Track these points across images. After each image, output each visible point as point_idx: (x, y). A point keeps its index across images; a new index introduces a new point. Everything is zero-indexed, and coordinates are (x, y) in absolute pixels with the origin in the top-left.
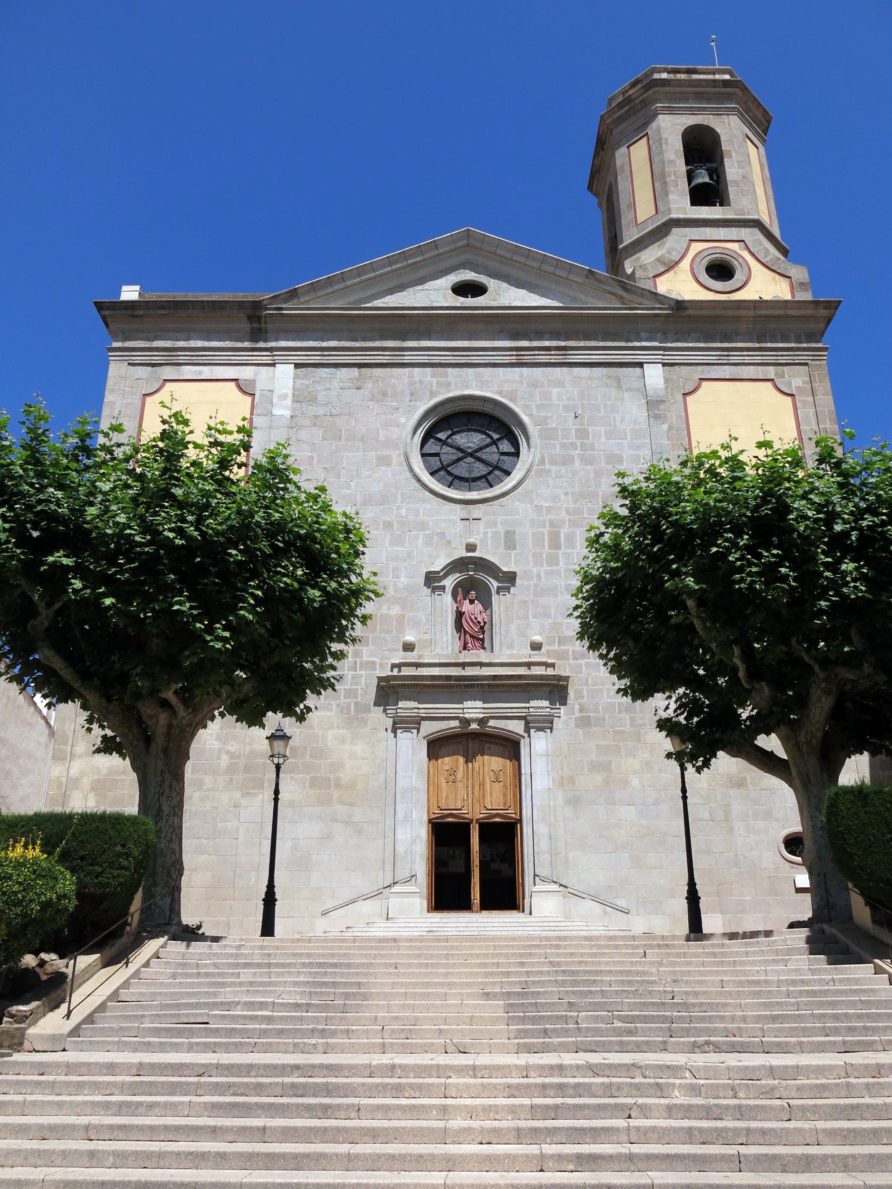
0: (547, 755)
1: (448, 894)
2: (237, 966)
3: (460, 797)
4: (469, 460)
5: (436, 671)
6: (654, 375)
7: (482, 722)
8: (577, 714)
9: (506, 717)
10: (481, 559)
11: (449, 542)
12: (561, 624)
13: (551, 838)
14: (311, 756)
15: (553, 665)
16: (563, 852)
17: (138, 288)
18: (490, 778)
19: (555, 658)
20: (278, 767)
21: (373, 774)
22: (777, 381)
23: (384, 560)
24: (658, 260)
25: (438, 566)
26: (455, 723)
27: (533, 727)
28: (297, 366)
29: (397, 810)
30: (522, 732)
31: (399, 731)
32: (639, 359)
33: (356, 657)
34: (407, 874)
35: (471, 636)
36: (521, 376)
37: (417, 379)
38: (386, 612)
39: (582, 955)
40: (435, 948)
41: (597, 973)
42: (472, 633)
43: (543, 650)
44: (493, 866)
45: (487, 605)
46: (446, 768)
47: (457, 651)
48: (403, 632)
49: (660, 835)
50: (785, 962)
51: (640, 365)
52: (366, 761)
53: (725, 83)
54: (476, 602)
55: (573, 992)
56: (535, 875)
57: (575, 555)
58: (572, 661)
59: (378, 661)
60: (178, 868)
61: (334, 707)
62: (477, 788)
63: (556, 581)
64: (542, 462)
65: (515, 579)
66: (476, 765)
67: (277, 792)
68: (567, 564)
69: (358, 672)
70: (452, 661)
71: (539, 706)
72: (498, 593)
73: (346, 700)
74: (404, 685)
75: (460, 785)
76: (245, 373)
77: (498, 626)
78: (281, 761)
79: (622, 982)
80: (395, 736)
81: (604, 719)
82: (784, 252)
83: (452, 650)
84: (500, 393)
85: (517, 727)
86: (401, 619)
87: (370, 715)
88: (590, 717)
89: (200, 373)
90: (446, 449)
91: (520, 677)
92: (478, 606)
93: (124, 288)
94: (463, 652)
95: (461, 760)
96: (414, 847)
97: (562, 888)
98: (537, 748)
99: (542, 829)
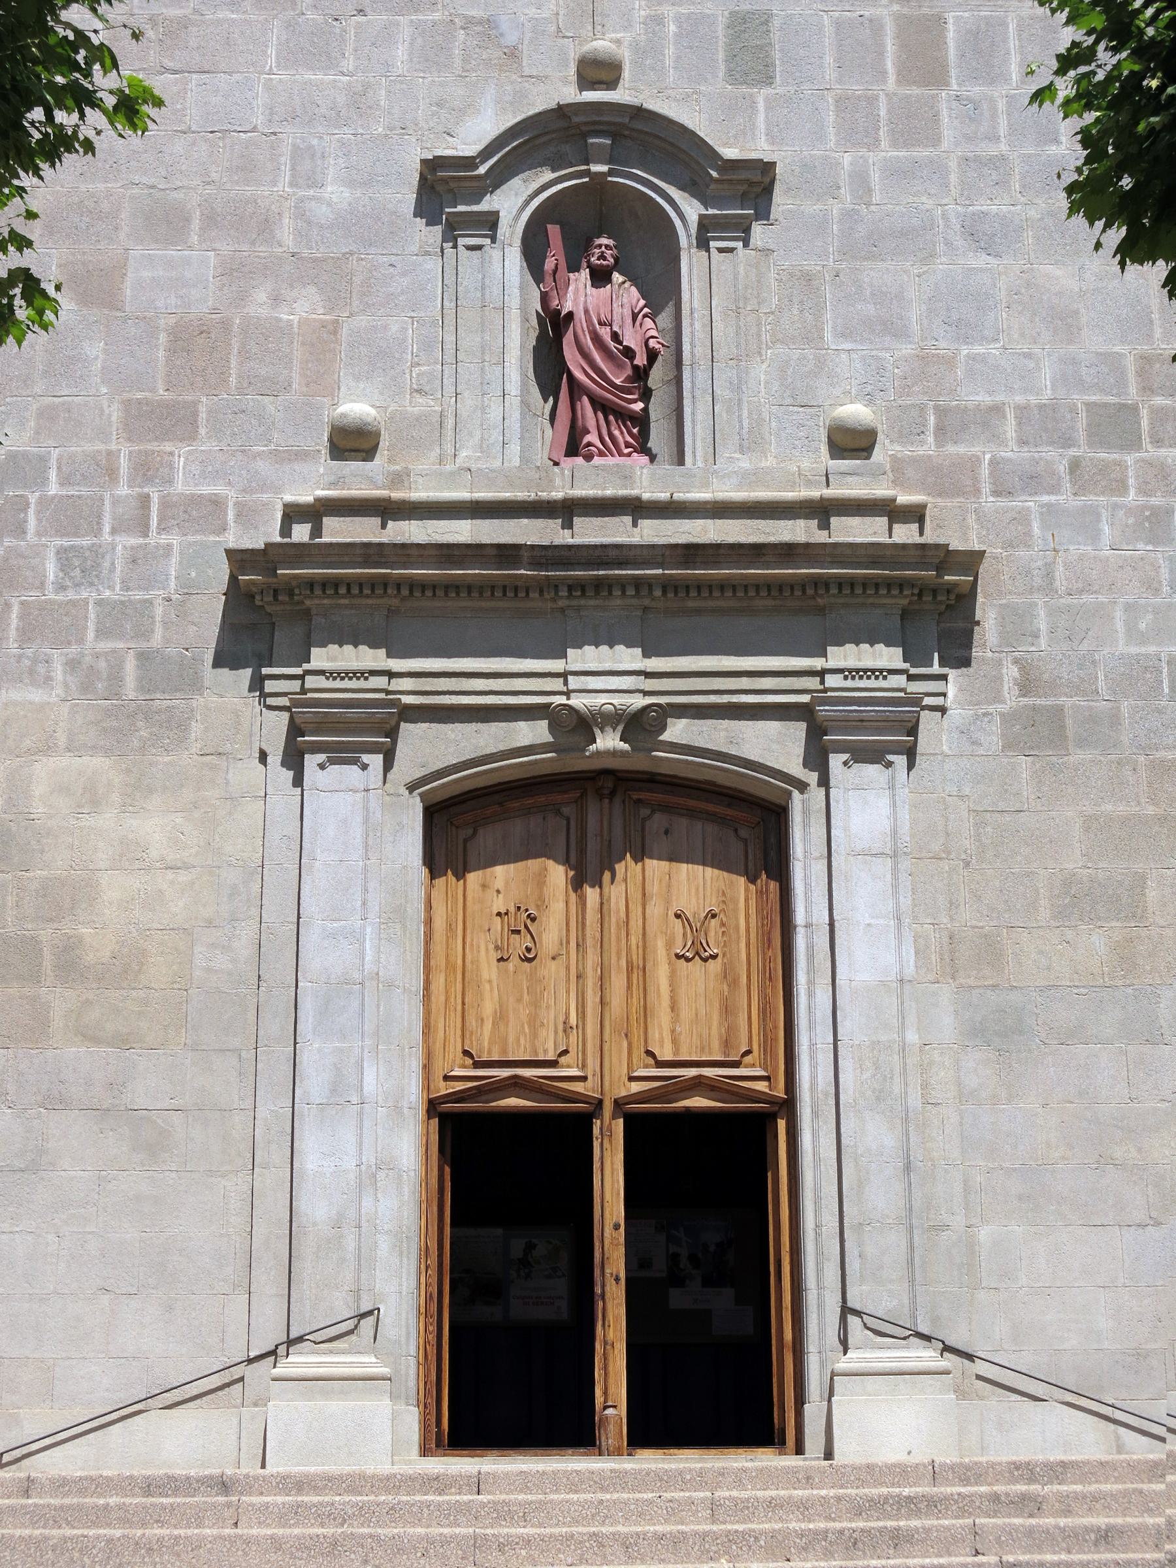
0: (895, 855)
1: (501, 1382)
3: (551, 1017)
5: (461, 531)
7: (641, 725)
8: (1011, 699)
9: (731, 709)
10: (639, 113)
11: (513, 54)
12: (950, 362)
13: (908, 1168)
15: (916, 514)
16: (958, 1221)
18: (669, 945)
19: (923, 487)
21: (210, 924)
23: (259, 120)
25: (472, 135)
26: (534, 732)
27: (841, 748)
29: (304, 1058)
30: (794, 765)
31: (311, 761)
33: (148, 480)
34: (342, 1307)
35: (600, 405)
38: (264, 312)
40: (416, 1514)
42: (601, 393)
43: (878, 455)
44: (678, 1299)
45: (661, 291)
46: (499, 905)
47: (541, 456)
48: (332, 391)
52: (183, 877)
54: (617, 277)
56: (846, 1310)
57: (1001, 105)
58: (988, 501)
59: (231, 495)
61: (58, 673)
62: (618, 982)
63: (929, 203)
65: (768, 190)
66: (616, 893)
68: (969, 139)
69: (155, 538)
70: (521, 495)
71: (866, 662)
72: (703, 243)
73: (106, 645)
74: (334, 584)
75: (551, 971)
77: (704, 364)
80: (298, 781)
81: (1115, 720)
83: (524, 459)
85: (776, 746)
86: (323, 341)
87: (199, 701)
88: (1060, 710)
91: (788, 552)
92: (624, 296)
94: (568, 463)
95: (558, 874)
96: (367, 1203)
97: (949, 1362)
98: (855, 822)
99: (872, 1134)
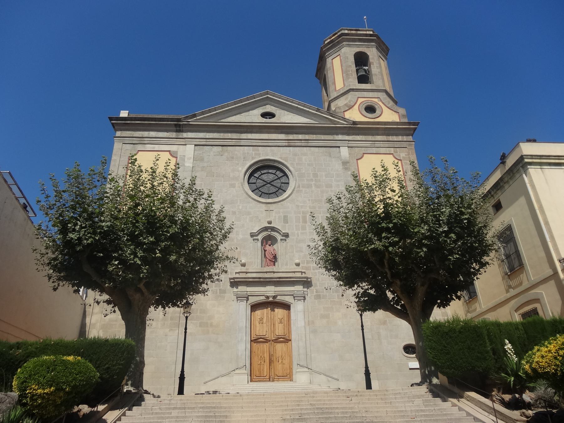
2: (170, 409)
4: (269, 185)
5: (254, 275)
6: (344, 152)
7: (274, 297)
9: (283, 293)
10: (274, 227)
14: (200, 313)
17: (128, 112)
20: (187, 318)
22: (395, 154)
24: (345, 105)
25: (255, 230)
26: (263, 298)
28: (195, 145)
32: (338, 145)
36: (290, 151)
37: (246, 152)
39: (324, 400)
41: (331, 408)
49: (354, 345)
50: (413, 402)
51: (339, 147)
53: (371, 35)
55: (323, 418)
60: (142, 364)
64: (299, 187)
67: (186, 329)
75: (265, 325)
76: (173, 148)
78: (188, 315)
79: (343, 413)
82: (396, 103)
84: (281, 158)
89: (154, 148)
90: (259, 181)
93: (122, 112)
98: (297, 307)
